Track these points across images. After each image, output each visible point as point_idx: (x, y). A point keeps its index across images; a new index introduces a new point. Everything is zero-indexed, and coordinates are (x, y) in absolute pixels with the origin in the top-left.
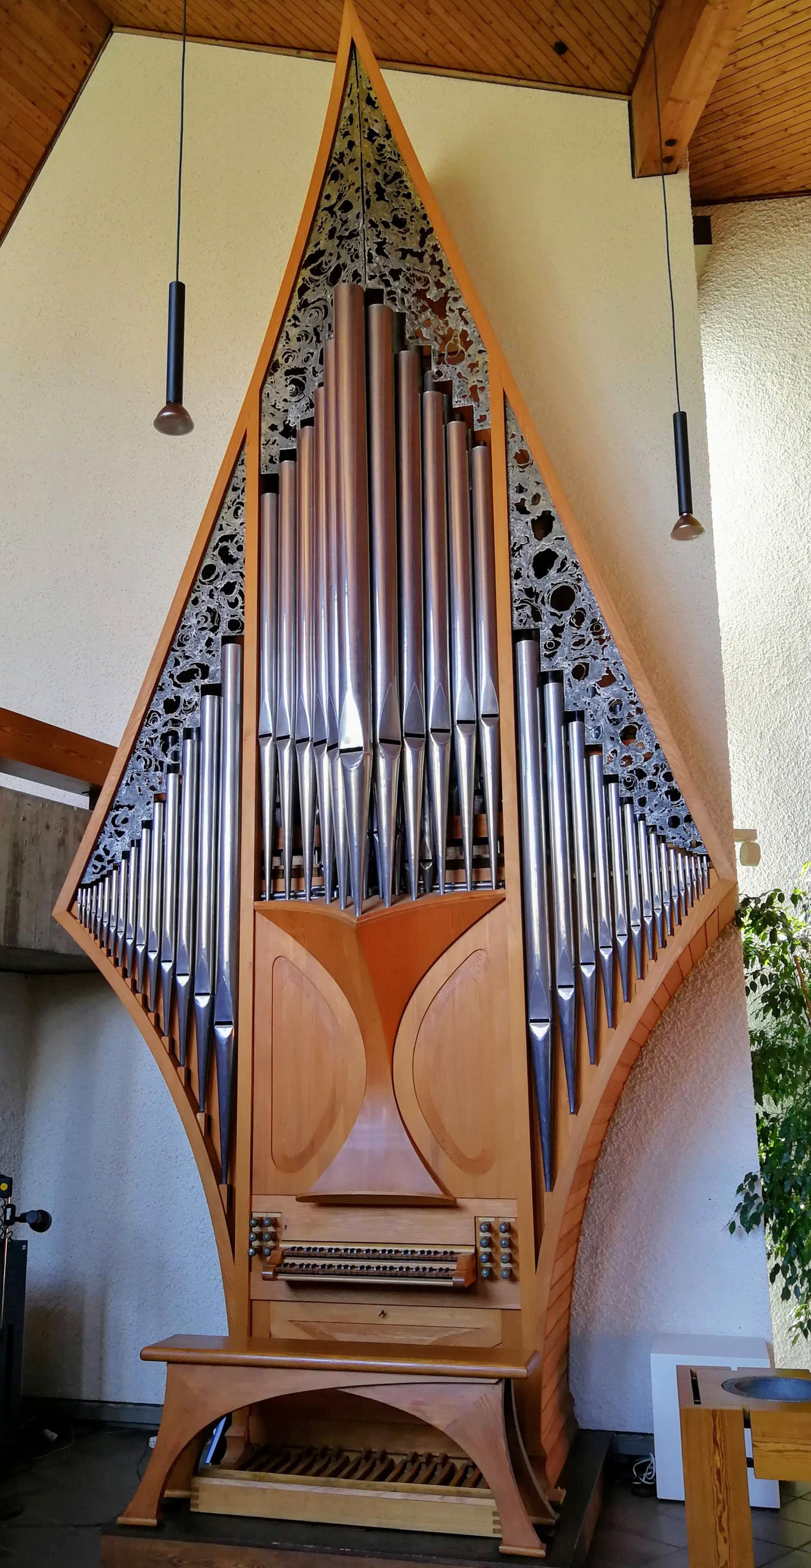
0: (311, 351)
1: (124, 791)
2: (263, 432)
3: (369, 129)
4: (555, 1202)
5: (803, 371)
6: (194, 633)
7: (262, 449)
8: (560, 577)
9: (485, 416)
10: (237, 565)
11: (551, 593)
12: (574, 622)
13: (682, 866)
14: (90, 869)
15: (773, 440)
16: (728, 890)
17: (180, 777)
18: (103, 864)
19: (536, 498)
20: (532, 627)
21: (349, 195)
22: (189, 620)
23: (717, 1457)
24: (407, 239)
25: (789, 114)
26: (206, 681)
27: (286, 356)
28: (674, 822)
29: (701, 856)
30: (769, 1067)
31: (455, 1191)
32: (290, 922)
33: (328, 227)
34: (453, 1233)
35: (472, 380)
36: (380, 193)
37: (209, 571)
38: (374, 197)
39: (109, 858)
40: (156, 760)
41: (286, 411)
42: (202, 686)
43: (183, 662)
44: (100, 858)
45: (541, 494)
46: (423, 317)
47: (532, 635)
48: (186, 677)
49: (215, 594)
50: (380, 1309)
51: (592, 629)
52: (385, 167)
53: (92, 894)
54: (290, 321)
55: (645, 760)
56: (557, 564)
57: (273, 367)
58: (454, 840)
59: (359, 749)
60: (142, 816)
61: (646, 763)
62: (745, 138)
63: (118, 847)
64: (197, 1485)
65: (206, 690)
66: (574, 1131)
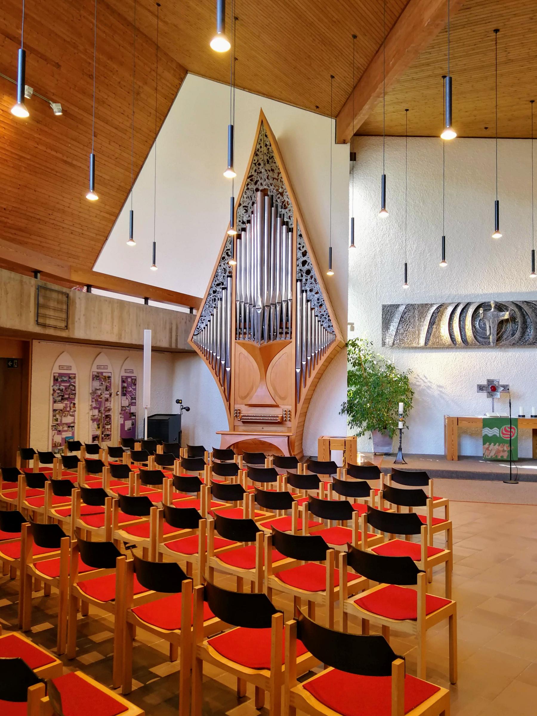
1: (203, 312)
4: (299, 406)
16: (250, 408)
19: (303, 247)
21: (260, 161)
28: (329, 326)
30: (352, 379)
31: (278, 404)
32: (243, 345)
33: (254, 169)
34: (278, 412)
35: (289, 214)
36: (268, 162)
37: (223, 258)
38: (266, 163)
44: (198, 328)
46: (278, 196)
47: (301, 281)
58: (281, 328)
63: (203, 326)
65: (223, 289)
66: (304, 391)
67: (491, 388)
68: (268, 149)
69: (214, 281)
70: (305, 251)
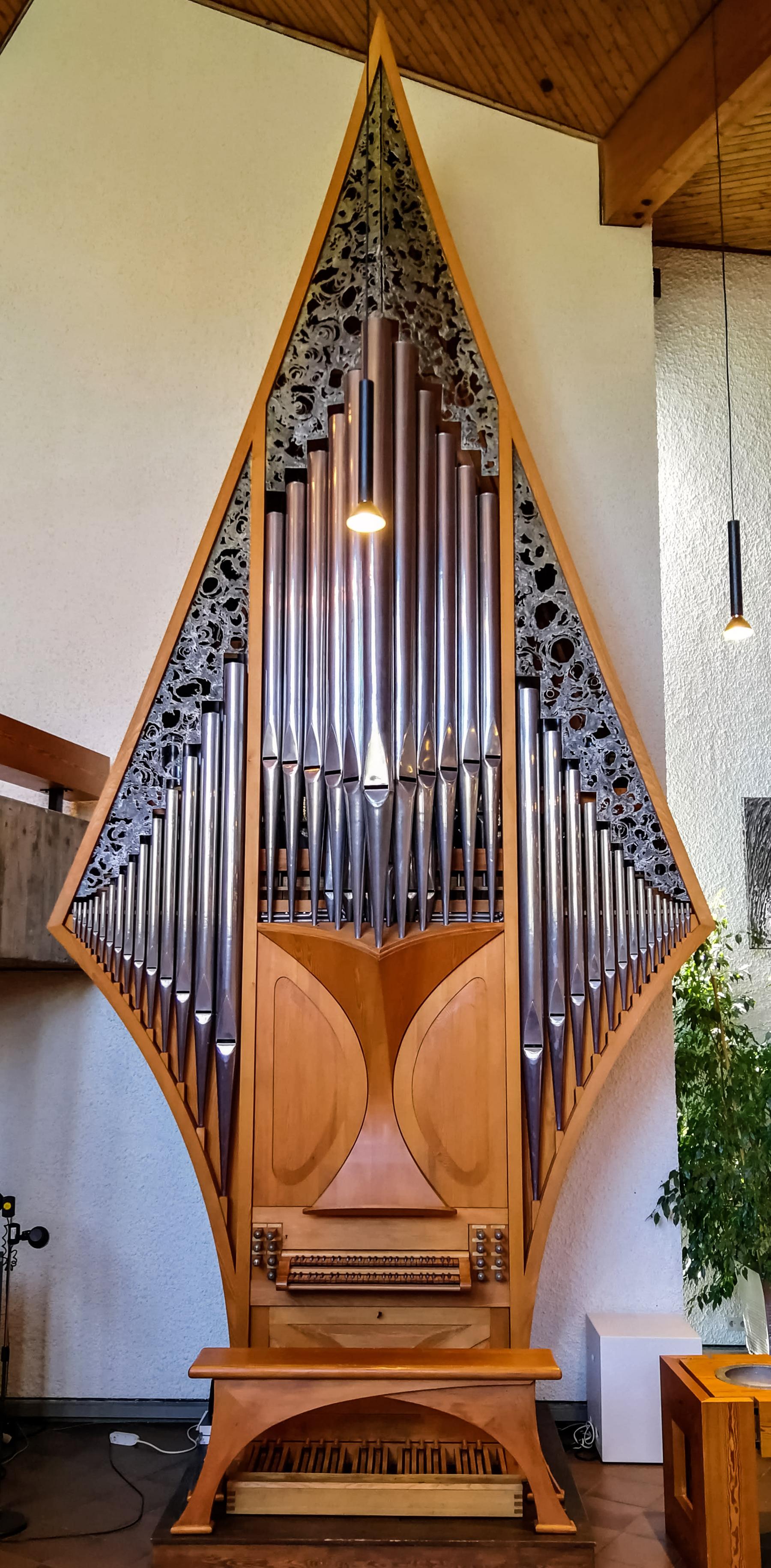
0: (321, 371)
1: (120, 804)
2: (268, 447)
3: (389, 152)
5: (715, 422)
6: (194, 647)
7: (268, 465)
8: (561, 630)
9: (493, 463)
10: (240, 581)
11: (552, 644)
12: (573, 674)
13: (666, 911)
14: (85, 883)
15: (686, 484)
17: (180, 793)
18: (99, 877)
19: (540, 551)
20: (534, 675)
22: (189, 633)
23: (732, 1441)
24: (422, 273)
25: (737, 184)
26: (207, 698)
27: (293, 371)
29: (685, 903)
32: (296, 946)
33: (342, 245)
34: (447, 1241)
35: (481, 426)
36: (398, 220)
37: (210, 584)
38: (391, 224)
39: (106, 872)
40: (155, 775)
41: (292, 428)
42: (203, 702)
43: (182, 676)
44: (95, 872)
45: (544, 546)
47: (533, 683)
48: (186, 691)
49: (218, 609)
50: (378, 1310)
51: (589, 683)
52: (403, 194)
53: (88, 908)
54: (298, 335)
55: (635, 811)
56: (558, 617)
57: (280, 381)
59: (384, 787)
60: (140, 830)
61: (636, 814)
62: (691, 195)
63: (116, 861)
64: (233, 1490)
65: (208, 707)
67: (6, 824)
68: (400, 173)
69: (170, 676)
70: (549, 567)
